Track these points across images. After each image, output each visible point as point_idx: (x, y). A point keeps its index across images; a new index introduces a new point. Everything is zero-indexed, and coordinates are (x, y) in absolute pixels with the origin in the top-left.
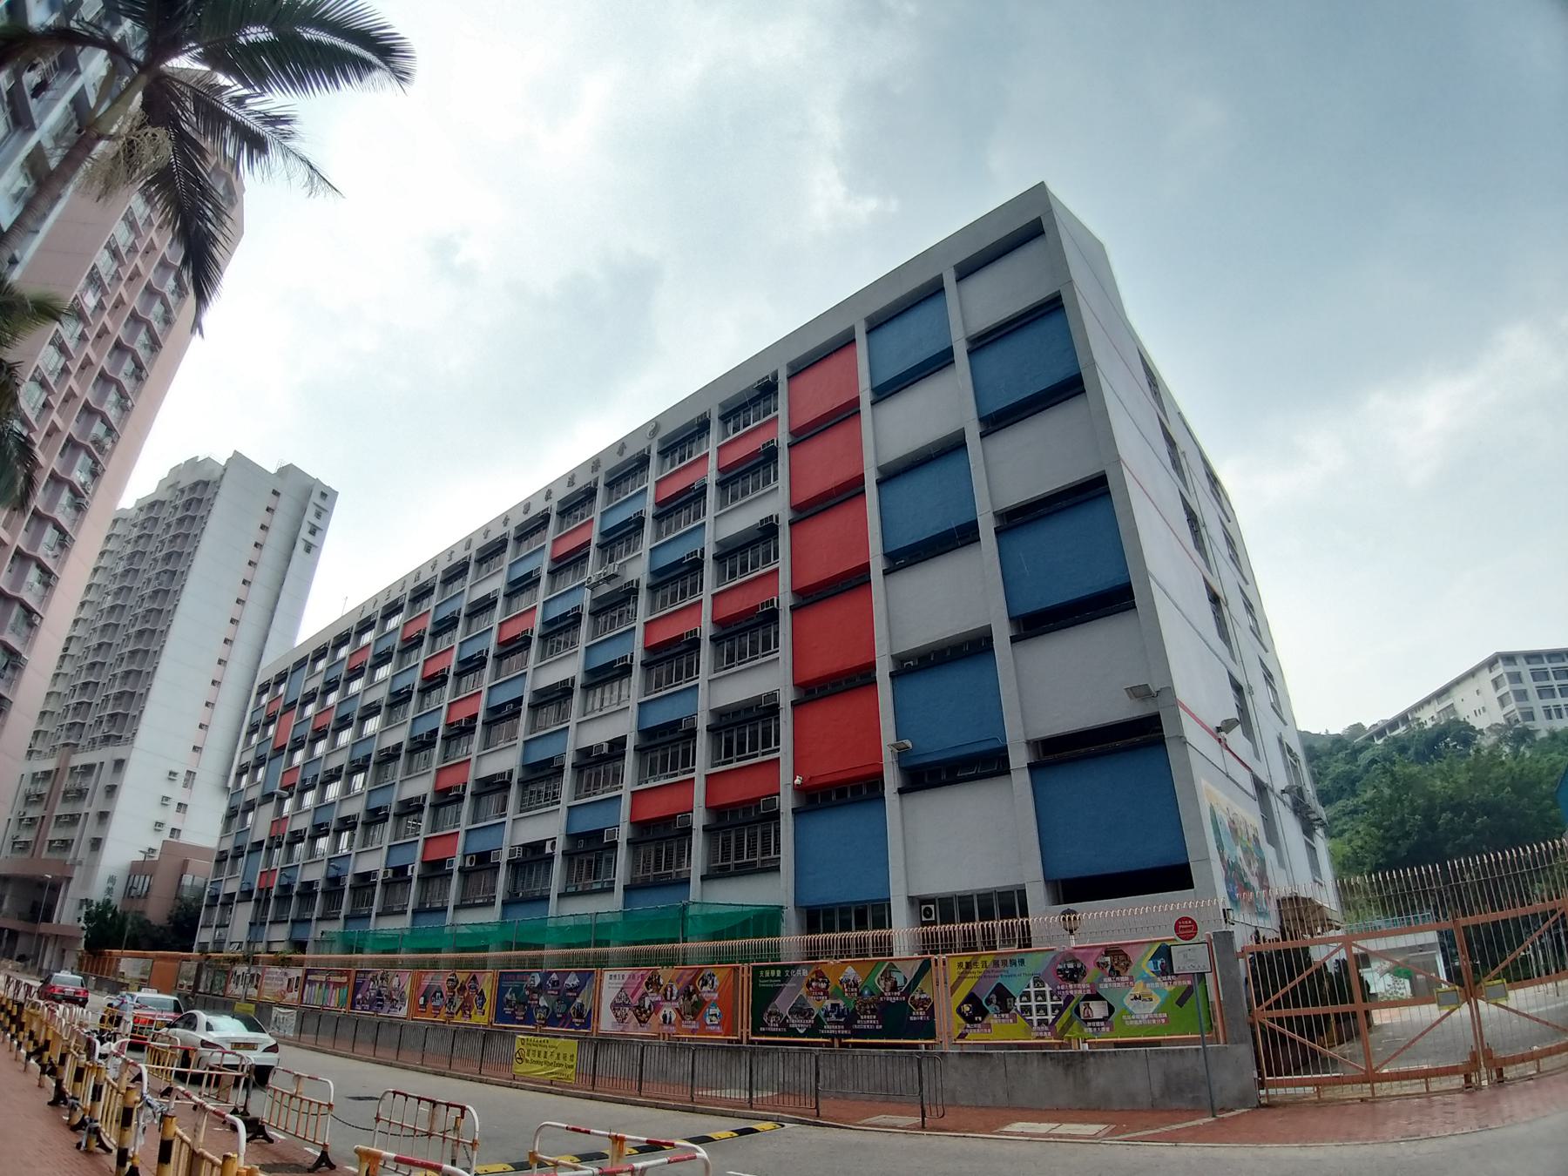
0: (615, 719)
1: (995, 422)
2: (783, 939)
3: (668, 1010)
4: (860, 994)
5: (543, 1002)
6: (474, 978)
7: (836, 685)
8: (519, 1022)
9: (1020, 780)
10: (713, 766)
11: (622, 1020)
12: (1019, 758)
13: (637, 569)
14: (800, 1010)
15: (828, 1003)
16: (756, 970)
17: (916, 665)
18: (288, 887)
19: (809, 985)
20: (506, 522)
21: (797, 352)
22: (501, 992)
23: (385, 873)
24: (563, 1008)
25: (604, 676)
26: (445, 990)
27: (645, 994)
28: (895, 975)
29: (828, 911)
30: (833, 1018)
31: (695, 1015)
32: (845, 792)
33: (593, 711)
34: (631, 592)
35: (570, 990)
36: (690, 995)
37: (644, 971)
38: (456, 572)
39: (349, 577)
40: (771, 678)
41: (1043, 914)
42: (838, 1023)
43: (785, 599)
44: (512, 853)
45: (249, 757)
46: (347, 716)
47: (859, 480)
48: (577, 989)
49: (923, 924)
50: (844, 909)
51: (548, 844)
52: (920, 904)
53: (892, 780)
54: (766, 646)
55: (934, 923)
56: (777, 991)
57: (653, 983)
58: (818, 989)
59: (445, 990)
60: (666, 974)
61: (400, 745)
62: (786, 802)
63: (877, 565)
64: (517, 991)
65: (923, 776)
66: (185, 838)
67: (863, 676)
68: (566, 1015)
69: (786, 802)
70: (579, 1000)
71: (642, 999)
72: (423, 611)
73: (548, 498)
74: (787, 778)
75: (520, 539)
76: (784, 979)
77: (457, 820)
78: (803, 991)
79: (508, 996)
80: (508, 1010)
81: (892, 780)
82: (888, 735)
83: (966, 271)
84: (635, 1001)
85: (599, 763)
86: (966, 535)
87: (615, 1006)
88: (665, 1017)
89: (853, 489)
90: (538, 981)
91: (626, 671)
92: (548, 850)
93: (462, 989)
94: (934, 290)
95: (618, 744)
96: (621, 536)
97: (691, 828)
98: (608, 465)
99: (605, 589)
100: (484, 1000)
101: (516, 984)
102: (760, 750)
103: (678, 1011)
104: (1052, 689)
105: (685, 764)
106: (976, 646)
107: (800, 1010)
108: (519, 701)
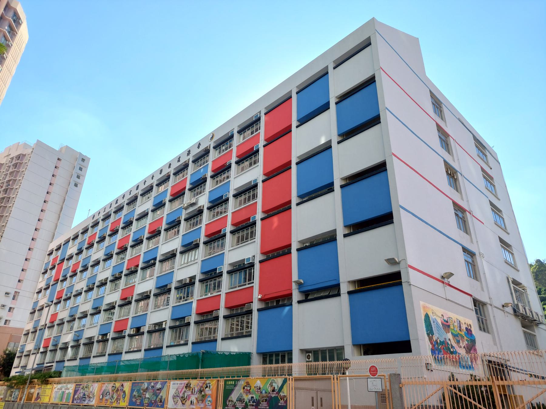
0: (189, 268)
1: (347, 135)
2: (251, 367)
3: (193, 398)
4: (261, 393)
5: (147, 396)
6: (122, 385)
7: (277, 253)
8: (138, 405)
9: (344, 298)
10: (229, 289)
11: (176, 403)
12: (345, 288)
13: (203, 201)
14: (240, 400)
15: (250, 396)
16: (226, 381)
17: (312, 244)
18: (56, 345)
19: (244, 388)
20: (189, 152)
21: (338, 54)
22: (132, 391)
23: (98, 337)
24: (155, 398)
25: (190, 247)
26: (111, 391)
27: (185, 391)
28: (274, 384)
29: (271, 354)
30: (251, 403)
31: (202, 401)
32: (277, 301)
33: (191, 261)
34: (200, 212)
35: (158, 390)
36: (201, 392)
37: (185, 382)
38: (133, 201)
39: (93, 200)
40: (251, 251)
41: (256, 366)
42: (253, 405)
43: (259, 215)
44: (149, 327)
45: (43, 285)
46: (86, 265)
47: (290, 163)
48: (160, 389)
49: (307, 362)
50: (277, 354)
51: (164, 323)
52: (305, 352)
53: (296, 296)
54: (251, 237)
55: (311, 361)
56: (232, 390)
57: (188, 386)
58: (247, 390)
59: (111, 391)
60: (194, 383)
61: (107, 278)
62: (256, 305)
63: (295, 200)
64: (138, 391)
65: (309, 296)
66: (12, 325)
67: (286, 250)
68: (155, 401)
69: (256, 305)
70: (161, 394)
71: (184, 393)
72: (117, 219)
73: (188, 154)
74: (257, 295)
75: (158, 185)
76: (235, 385)
77: (129, 313)
78: (242, 391)
79: (135, 393)
80: (134, 400)
81: (296, 296)
82: (295, 277)
83: (338, 64)
84: (181, 395)
85: (186, 286)
86: (329, 188)
87: (174, 397)
88: (191, 402)
89: (287, 166)
90: (146, 385)
91: (197, 246)
92: (164, 326)
93: (118, 390)
94: (324, 74)
95: (192, 278)
96: (199, 184)
97: (252, 310)
98: (193, 153)
99: (191, 209)
100: (125, 395)
101: (138, 388)
102: (247, 282)
103: (196, 399)
104: (359, 257)
105: (250, 280)
106: (330, 238)
107: (240, 400)
108: (155, 259)
